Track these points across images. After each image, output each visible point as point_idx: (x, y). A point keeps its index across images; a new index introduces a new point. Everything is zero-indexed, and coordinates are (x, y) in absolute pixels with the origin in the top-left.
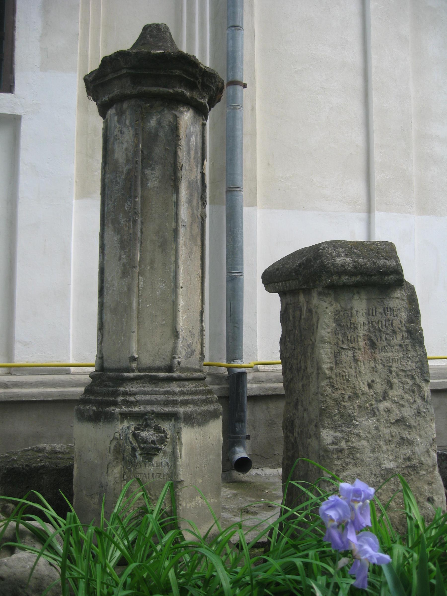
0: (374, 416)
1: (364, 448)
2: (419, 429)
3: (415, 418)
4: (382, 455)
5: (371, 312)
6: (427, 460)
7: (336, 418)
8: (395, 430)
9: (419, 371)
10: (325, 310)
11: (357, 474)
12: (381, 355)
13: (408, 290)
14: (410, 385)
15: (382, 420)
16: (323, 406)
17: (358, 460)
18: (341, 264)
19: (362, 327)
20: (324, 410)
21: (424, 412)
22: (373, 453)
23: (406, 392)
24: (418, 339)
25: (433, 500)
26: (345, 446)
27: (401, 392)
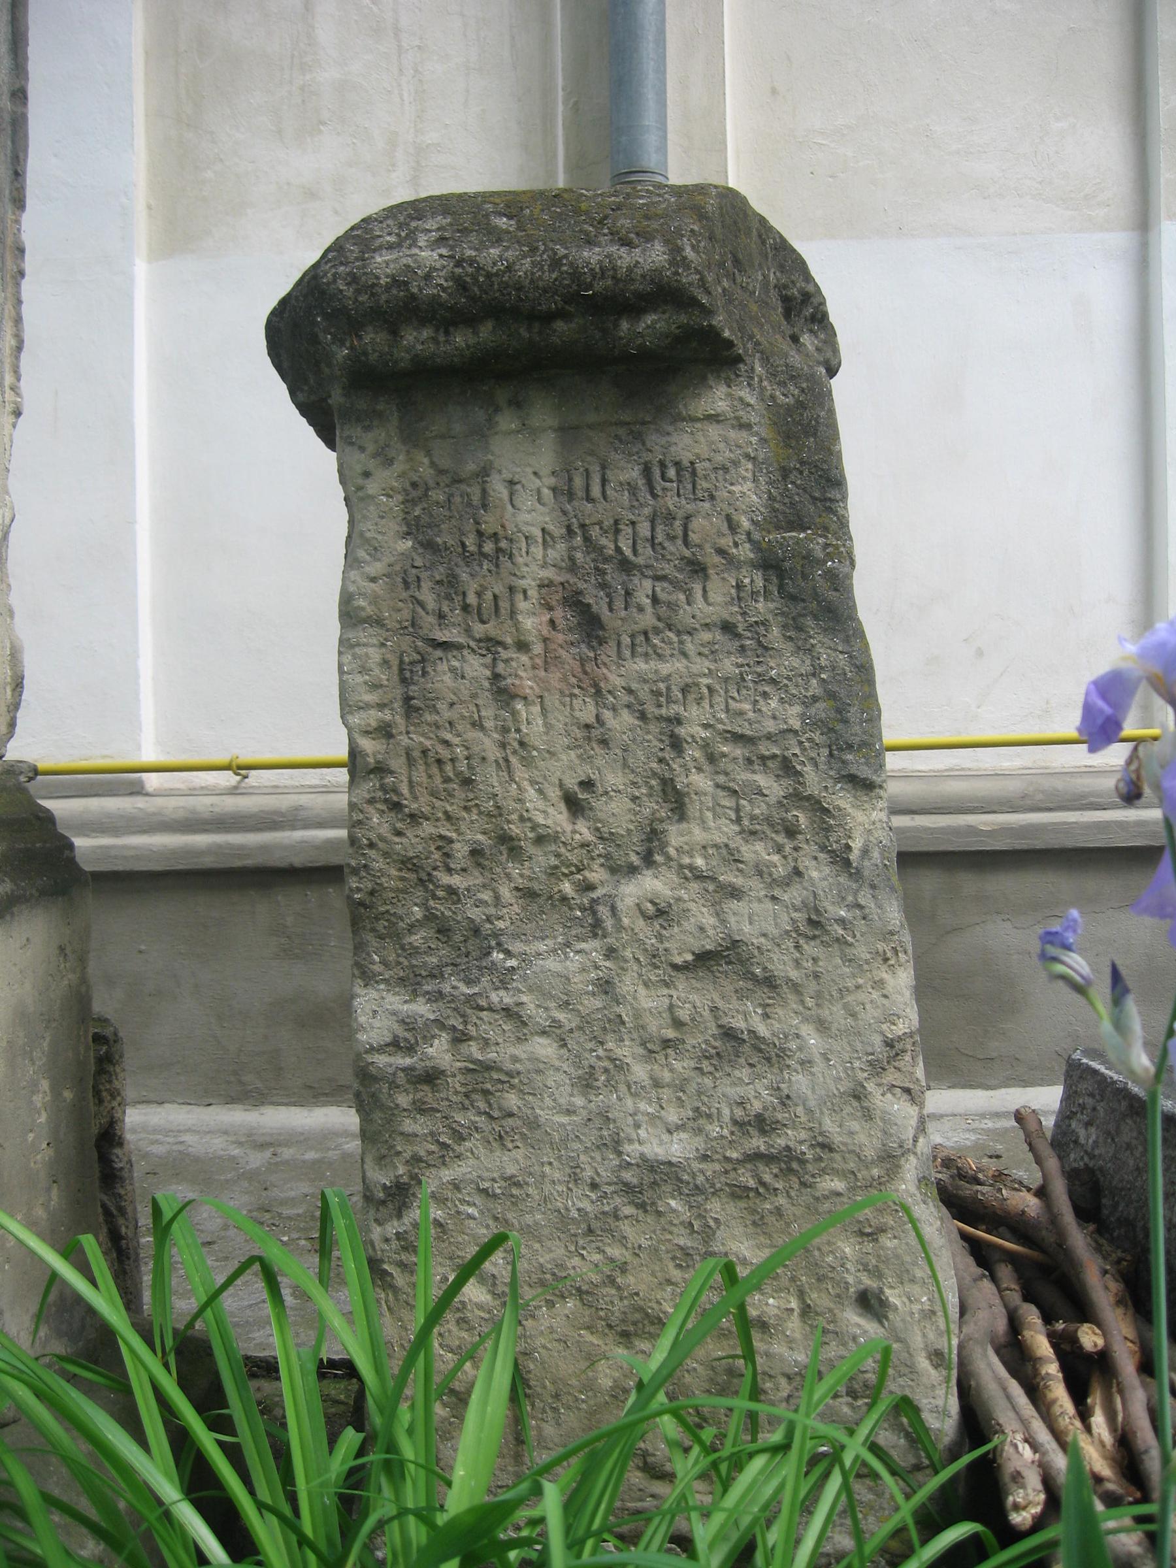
0: (595, 935)
1: (539, 1072)
2: (818, 996)
3: (798, 947)
4: (629, 1102)
5: (578, 482)
6: (851, 1133)
7: (416, 939)
8: (695, 997)
9: (817, 737)
10: (360, 481)
11: (505, 1179)
12: (625, 672)
13: (782, 384)
14: (772, 800)
15: (628, 954)
16: (359, 890)
17: (510, 1121)
18: (393, 277)
19: (538, 551)
20: (361, 904)
21: (842, 921)
22: (585, 1095)
23: (753, 833)
24: (816, 596)
25: (884, 1303)
26: (448, 1057)
27: (724, 831)
